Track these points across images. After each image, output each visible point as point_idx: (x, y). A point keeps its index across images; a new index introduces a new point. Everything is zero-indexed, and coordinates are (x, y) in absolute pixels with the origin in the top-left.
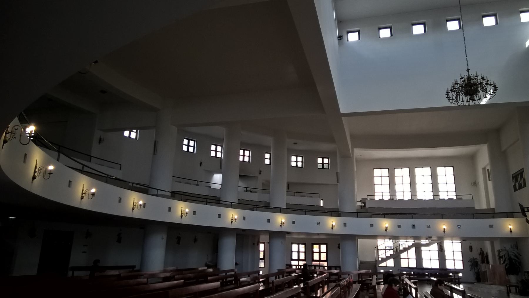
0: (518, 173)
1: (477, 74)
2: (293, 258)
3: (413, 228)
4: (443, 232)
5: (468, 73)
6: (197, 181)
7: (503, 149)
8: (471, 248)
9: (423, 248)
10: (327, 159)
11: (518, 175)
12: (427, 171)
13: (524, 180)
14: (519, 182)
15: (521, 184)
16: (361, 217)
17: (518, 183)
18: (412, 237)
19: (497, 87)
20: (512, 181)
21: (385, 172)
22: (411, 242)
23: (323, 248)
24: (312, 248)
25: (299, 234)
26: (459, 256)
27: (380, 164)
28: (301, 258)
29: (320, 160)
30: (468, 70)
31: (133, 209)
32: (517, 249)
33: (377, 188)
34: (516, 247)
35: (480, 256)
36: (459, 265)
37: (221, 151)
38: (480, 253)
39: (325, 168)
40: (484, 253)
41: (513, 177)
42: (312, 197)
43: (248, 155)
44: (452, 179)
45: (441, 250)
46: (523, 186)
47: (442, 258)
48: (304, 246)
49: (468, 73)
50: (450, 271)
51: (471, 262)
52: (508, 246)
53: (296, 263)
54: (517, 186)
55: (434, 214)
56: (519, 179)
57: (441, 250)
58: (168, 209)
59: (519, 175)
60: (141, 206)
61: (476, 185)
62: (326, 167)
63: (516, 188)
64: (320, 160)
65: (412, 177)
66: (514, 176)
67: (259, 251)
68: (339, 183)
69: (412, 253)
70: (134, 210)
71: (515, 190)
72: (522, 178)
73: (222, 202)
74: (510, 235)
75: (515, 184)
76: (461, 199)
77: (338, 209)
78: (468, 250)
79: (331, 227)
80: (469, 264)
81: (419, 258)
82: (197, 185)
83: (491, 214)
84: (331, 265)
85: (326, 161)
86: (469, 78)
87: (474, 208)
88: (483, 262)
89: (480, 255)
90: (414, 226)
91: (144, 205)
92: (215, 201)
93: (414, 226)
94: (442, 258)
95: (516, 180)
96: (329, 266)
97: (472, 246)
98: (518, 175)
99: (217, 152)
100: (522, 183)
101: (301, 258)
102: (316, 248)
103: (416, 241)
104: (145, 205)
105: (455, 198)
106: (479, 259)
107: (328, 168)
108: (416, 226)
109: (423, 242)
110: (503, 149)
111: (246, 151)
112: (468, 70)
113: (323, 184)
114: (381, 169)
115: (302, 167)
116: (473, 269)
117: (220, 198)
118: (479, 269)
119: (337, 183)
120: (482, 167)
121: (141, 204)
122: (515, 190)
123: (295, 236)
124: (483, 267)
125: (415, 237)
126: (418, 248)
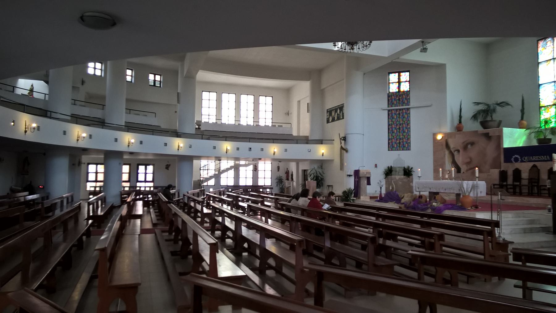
0: (333, 109)
2: (90, 179)
3: (261, 151)
4: (24, 131)
6: (130, 110)
7: (323, 87)
8: (278, 168)
9: (241, 168)
10: (159, 76)
11: (333, 111)
12: (251, 98)
13: (343, 114)
14: (333, 116)
15: (335, 117)
16: (105, 129)
17: (332, 117)
18: (232, 158)
20: (326, 116)
21: (213, 95)
22: (232, 163)
23: (150, 168)
24: (138, 169)
25: (146, 154)
26: (269, 174)
27: (210, 87)
28: (98, 179)
29: (151, 77)
31: (26, 132)
32: (322, 168)
33: (205, 111)
34: (321, 167)
35: (286, 174)
36: (268, 183)
37: (131, 75)
38: (286, 172)
39: (156, 85)
40: (289, 172)
41: (327, 112)
42: (146, 116)
43: (131, 74)
44: (270, 108)
45: (256, 169)
46: (336, 119)
47: (255, 177)
48: (128, 166)
50: (261, 187)
51: (278, 179)
52: (316, 166)
53: (143, 184)
54: (330, 119)
55: (262, 139)
56: (333, 113)
57: (256, 169)
58: (62, 133)
59: (334, 110)
60: (34, 129)
61: (288, 115)
62: (157, 84)
63: (329, 121)
64: (151, 77)
65: (238, 103)
66: (329, 111)
67: (121, 173)
68: (179, 103)
69: (232, 173)
70: (26, 133)
71: (328, 122)
72: (336, 113)
73: (106, 125)
74: (322, 158)
75: (329, 117)
76: (281, 126)
77: (176, 130)
78: (276, 169)
79: (76, 138)
80: (277, 181)
81: (237, 177)
82: (75, 104)
83: (306, 140)
84: (156, 185)
85: (158, 78)
87: (292, 134)
88: (288, 179)
89: (286, 173)
90: (251, 148)
91: (38, 128)
92: (101, 123)
93: (251, 148)
94: (255, 177)
95: (331, 114)
96: (156, 187)
97: (280, 166)
98: (333, 110)
99: (96, 70)
100: (336, 117)
101: (98, 179)
102: (142, 168)
103: (237, 162)
104: (39, 128)
105: (270, 125)
106: (284, 176)
107: (159, 86)
108: (252, 149)
109: (242, 162)
110: (323, 87)
111: (156, 76)
113: (158, 103)
114: (209, 92)
115: (131, 82)
116: (278, 185)
117: (104, 120)
118: (283, 185)
119: (178, 103)
120: (297, 100)
121: (34, 127)
122: (328, 122)
123: (142, 157)
124: (286, 184)
125: (235, 158)
126: (236, 168)
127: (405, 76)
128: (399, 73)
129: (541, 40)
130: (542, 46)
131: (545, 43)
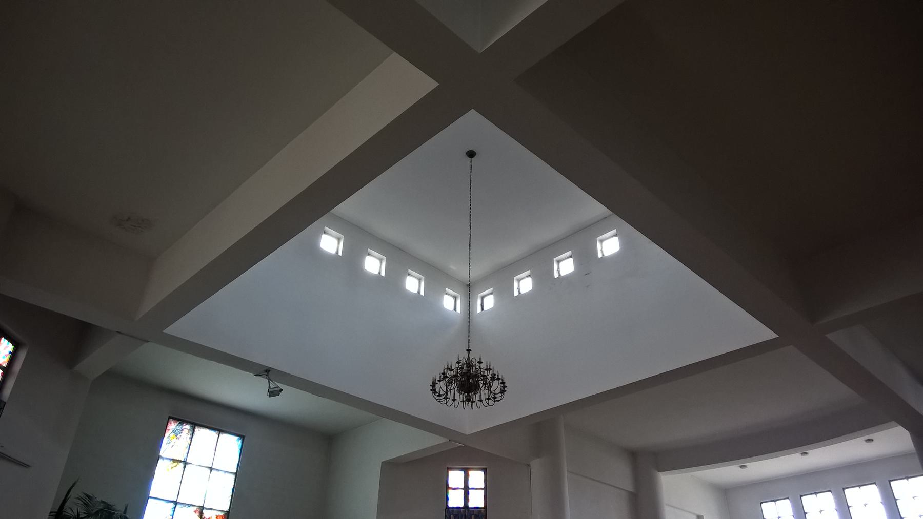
1: (480, 359)
5: (469, 355)
19: (506, 387)
30: (469, 351)
49: (469, 355)
86: (469, 365)
112: (469, 351)
127: (477, 478)
128: (466, 471)
129: (176, 419)
130: (174, 432)
131: (179, 428)
